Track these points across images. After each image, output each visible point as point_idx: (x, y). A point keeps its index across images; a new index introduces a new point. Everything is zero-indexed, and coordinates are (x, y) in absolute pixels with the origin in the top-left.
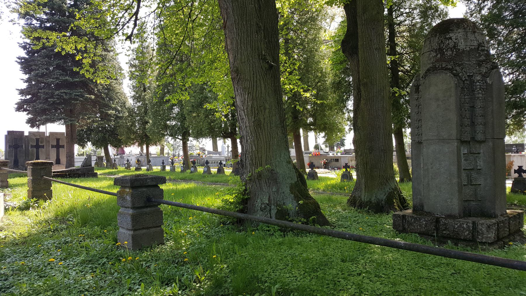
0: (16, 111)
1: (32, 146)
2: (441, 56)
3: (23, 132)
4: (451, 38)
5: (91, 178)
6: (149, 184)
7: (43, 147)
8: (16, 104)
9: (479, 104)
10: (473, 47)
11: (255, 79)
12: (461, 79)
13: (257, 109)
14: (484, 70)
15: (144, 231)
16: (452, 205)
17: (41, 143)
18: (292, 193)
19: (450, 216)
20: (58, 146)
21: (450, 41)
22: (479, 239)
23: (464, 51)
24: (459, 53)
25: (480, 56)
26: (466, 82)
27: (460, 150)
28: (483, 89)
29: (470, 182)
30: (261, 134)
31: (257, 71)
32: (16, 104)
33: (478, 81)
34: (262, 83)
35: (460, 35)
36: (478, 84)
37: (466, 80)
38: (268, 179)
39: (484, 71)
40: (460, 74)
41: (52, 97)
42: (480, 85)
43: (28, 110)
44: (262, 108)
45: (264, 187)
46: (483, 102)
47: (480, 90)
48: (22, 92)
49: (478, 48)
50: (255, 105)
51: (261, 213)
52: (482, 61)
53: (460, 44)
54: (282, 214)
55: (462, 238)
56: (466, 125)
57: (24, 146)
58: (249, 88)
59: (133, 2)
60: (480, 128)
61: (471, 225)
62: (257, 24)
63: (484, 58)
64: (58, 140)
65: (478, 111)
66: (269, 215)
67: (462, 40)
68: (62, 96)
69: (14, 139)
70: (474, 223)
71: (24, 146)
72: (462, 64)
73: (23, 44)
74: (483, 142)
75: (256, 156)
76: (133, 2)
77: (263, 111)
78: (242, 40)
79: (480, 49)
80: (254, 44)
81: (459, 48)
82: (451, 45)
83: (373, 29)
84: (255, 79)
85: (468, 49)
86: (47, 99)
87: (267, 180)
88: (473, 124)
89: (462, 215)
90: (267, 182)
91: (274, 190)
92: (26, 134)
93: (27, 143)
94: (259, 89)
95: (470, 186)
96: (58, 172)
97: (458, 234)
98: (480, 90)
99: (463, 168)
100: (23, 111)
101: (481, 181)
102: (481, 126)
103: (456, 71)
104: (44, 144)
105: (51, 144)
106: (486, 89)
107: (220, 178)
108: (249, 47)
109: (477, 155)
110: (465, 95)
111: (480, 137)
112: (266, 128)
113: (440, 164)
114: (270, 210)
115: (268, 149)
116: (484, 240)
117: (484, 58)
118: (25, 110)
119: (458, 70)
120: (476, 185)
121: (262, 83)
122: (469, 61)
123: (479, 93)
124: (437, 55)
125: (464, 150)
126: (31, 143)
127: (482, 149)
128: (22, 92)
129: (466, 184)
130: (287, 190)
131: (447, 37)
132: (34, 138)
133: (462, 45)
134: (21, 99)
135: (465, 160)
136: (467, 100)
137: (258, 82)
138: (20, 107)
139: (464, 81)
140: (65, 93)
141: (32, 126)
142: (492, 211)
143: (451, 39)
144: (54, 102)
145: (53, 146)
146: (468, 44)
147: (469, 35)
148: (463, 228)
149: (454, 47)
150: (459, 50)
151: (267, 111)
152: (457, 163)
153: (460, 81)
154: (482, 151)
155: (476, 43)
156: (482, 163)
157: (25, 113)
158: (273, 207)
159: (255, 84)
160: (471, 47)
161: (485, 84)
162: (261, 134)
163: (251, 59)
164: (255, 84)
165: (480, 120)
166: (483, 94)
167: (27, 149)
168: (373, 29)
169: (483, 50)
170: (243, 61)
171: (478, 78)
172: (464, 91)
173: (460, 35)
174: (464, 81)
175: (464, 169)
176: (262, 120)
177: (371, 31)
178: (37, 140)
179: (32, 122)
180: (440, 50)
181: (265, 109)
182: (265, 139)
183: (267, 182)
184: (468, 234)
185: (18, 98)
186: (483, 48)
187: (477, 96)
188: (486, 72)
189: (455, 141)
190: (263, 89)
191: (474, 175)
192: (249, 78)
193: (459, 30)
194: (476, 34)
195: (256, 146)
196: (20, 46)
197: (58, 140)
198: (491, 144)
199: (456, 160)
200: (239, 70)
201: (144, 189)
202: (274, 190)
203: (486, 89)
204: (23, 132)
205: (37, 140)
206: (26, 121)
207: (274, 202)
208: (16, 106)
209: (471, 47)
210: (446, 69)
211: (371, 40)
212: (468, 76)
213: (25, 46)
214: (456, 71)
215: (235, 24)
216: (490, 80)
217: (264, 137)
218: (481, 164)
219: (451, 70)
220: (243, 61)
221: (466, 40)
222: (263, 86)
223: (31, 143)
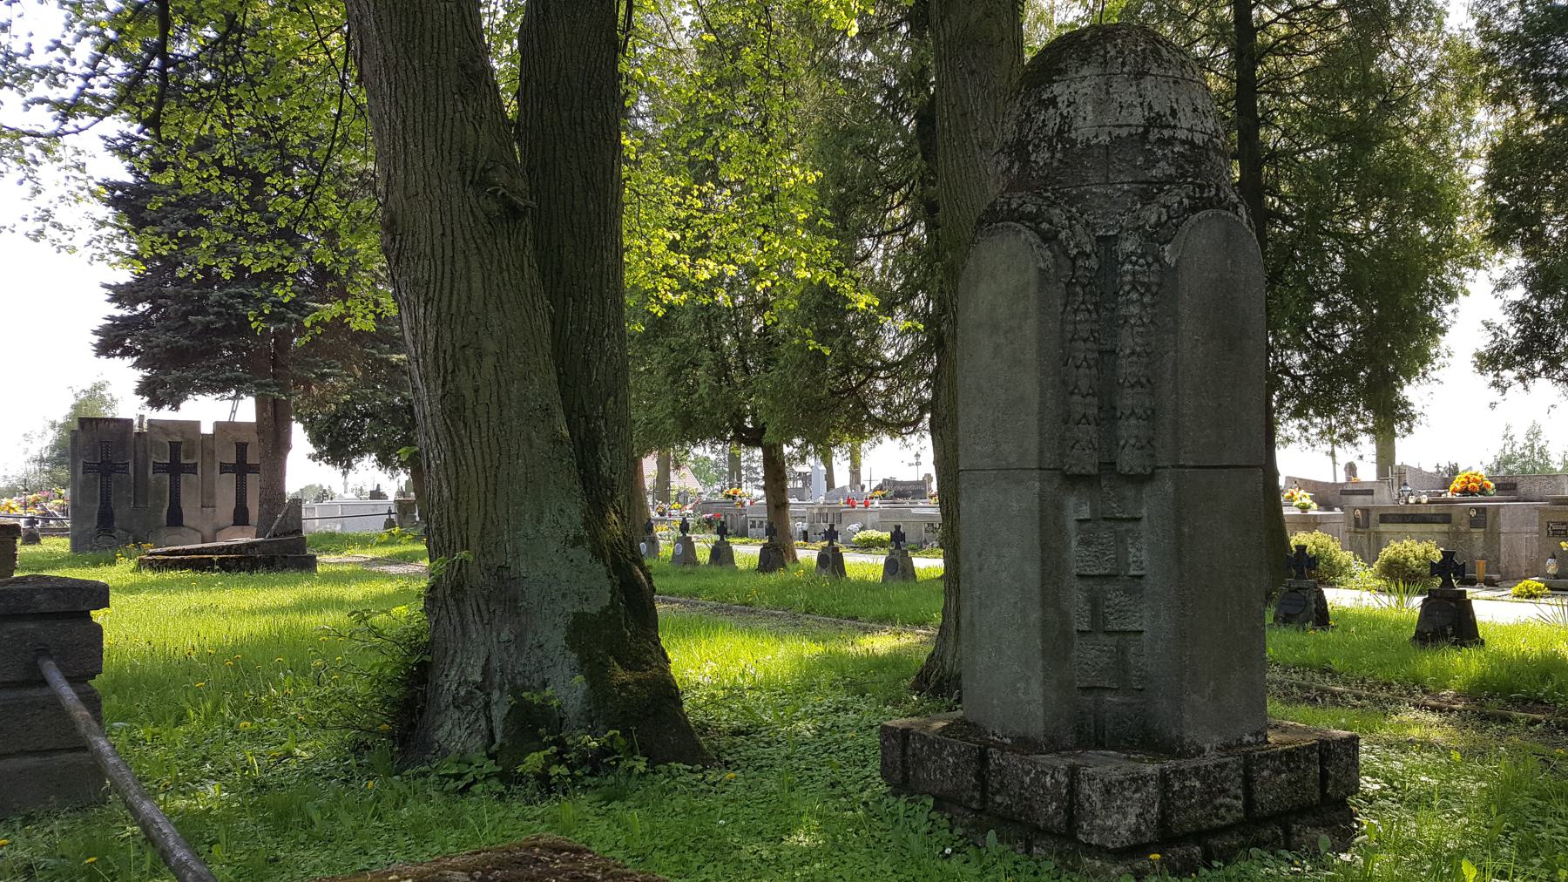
0: (98, 355)
1: (158, 468)
2: (1022, 168)
3: (196, 424)
4: (1053, 102)
5: (290, 575)
6: (44, 608)
7: (192, 469)
8: (96, 333)
9: (1128, 341)
10: (1124, 132)
11: (449, 253)
12: (1065, 253)
13: (453, 356)
14: (1152, 215)
15: (30, 761)
16: (1029, 703)
17: (187, 457)
18: (572, 649)
19: (1025, 744)
20: (241, 469)
21: (1051, 111)
22: (1088, 833)
23: (1089, 146)
24: (1074, 155)
25: (1151, 162)
26: (1080, 262)
27: (1059, 507)
28: (1148, 286)
29: (1098, 623)
30: (466, 441)
31: (457, 226)
32: (96, 333)
33: (1129, 256)
34: (475, 265)
35: (1085, 88)
36: (1128, 267)
37: (1082, 254)
38: (487, 602)
39: (1153, 219)
40: (1063, 235)
41: (201, 311)
42: (1134, 274)
43: (138, 352)
44: (469, 351)
45: (472, 627)
46: (1141, 335)
47: (1134, 288)
48: (120, 294)
49: (1146, 131)
50: (447, 342)
51: (457, 715)
52: (1160, 183)
53: (1079, 122)
54: (533, 722)
55: (1041, 824)
56: (1077, 417)
57: (131, 467)
58: (428, 283)
59: (1510, 5)
60: (1129, 429)
61: (1063, 779)
62: (463, 67)
63: (1172, 171)
64: (242, 448)
65: (1127, 368)
66: (483, 723)
67: (1090, 108)
68: (232, 306)
69: (93, 445)
70: (1073, 772)
71: (131, 467)
72: (1081, 197)
73: (119, 142)
74: (1150, 477)
75: (453, 518)
76: (1510, 5)
77: (472, 364)
78: (410, 121)
79: (1154, 135)
80: (447, 136)
81: (1073, 135)
82: (1053, 124)
83: (972, 73)
84: (449, 253)
85: (1104, 138)
86: (186, 314)
87: (481, 601)
88: (1108, 416)
89: (1069, 739)
90: (483, 607)
91: (504, 636)
92: (207, 429)
93: (140, 455)
94: (462, 286)
95: (1101, 637)
96: (188, 552)
97: (1031, 808)
98: (1134, 288)
99: (1075, 571)
100: (122, 355)
101: (1140, 619)
102: (1133, 421)
103: (1051, 223)
104: (197, 459)
105: (218, 460)
106: (1160, 285)
107: (722, 580)
108: (429, 142)
109: (1130, 525)
110: (1076, 311)
111: (1129, 460)
112: (483, 420)
113: (998, 557)
114: (487, 705)
115: (490, 495)
116: (1095, 840)
117: (1172, 171)
118: (126, 352)
119: (1055, 220)
120: (1125, 632)
121: (475, 265)
122: (1108, 183)
123: (1130, 302)
124: (1012, 163)
125: (1077, 508)
126: (154, 458)
127: (1150, 505)
128: (120, 294)
129: (1086, 628)
130: (555, 637)
131: (1045, 97)
132: (165, 440)
133: (1085, 128)
134: (112, 318)
135: (1085, 543)
136: (1084, 330)
137: (460, 264)
138: (111, 341)
139: (1074, 260)
140: (241, 295)
141: (156, 403)
142: (1175, 732)
143: (1055, 106)
144: (207, 328)
145: (224, 468)
146: (1107, 122)
147: (1117, 85)
148: (1044, 787)
149: (1060, 132)
150: (1073, 142)
151: (489, 362)
152: (1038, 552)
153: (1062, 260)
154: (1144, 512)
155: (1138, 117)
156: (1144, 556)
157: (129, 361)
158: (496, 695)
159: (447, 270)
160: (1117, 131)
161: (1155, 267)
162: (466, 441)
163: (435, 182)
164: (447, 270)
165: (1127, 400)
166: (1144, 306)
167: (141, 472)
168: (972, 73)
169: (1164, 142)
170: (412, 190)
171: (1129, 246)
172: (1075, 294)
173: (1085, 88)
174: (1074, 260)
175: (1080, 576)
176: (468, 394)
177: (964, 80)
178: (175, 448)
179: (152, 391)
180: (1019, 149)
181: (480, 355)
182: (479, 458)
183: (483, 607)
184: (1056, 813)
185: (105, 310)
186: (1167, 133)
187: (1123, 312)
188: (1158, 224)
189: (1035, 474)
190: (477, 284)
191: (1114, 596)
192: (428, 250)
193: (1085, 71)
194: (1148, 82)
195: (453, 484)
196: (109, 148)
197: (242, 448)
198: (1169, 486)
199: (1037, 543)
200: (399, 220)
201: (31, 626)
202: (504, 636)
203: (1160, 285)
204: (196, 424)
205: (175, 448)
206: (135, 385)
207: (540, 677)
208: (96, 339)
209: (1117, 131)
210: (1022, 218)
211: (964, 115)
212: (1099, 239)
213: (129, 146)
214: (1051, 223)
215: (386, 66)
216: (1172, 253)
217: (478, 452)
218: (1141, 556)
219: (1033, 220)
220: (412, 190)
221: (1101, 105)
222: (477, 277)
223: (154, 458)
